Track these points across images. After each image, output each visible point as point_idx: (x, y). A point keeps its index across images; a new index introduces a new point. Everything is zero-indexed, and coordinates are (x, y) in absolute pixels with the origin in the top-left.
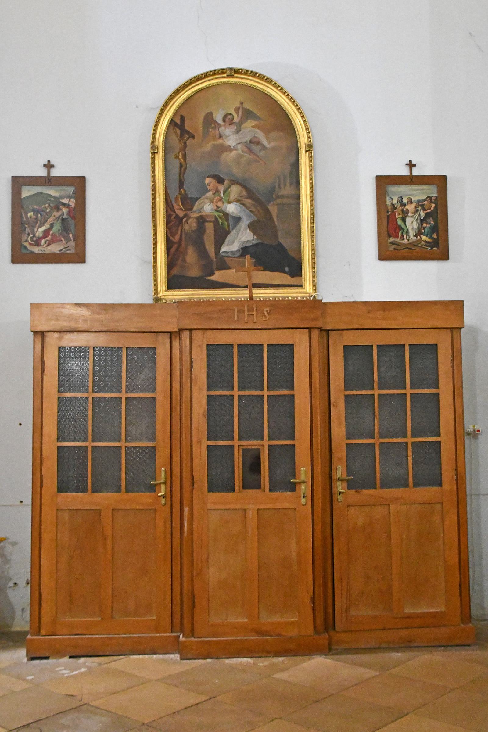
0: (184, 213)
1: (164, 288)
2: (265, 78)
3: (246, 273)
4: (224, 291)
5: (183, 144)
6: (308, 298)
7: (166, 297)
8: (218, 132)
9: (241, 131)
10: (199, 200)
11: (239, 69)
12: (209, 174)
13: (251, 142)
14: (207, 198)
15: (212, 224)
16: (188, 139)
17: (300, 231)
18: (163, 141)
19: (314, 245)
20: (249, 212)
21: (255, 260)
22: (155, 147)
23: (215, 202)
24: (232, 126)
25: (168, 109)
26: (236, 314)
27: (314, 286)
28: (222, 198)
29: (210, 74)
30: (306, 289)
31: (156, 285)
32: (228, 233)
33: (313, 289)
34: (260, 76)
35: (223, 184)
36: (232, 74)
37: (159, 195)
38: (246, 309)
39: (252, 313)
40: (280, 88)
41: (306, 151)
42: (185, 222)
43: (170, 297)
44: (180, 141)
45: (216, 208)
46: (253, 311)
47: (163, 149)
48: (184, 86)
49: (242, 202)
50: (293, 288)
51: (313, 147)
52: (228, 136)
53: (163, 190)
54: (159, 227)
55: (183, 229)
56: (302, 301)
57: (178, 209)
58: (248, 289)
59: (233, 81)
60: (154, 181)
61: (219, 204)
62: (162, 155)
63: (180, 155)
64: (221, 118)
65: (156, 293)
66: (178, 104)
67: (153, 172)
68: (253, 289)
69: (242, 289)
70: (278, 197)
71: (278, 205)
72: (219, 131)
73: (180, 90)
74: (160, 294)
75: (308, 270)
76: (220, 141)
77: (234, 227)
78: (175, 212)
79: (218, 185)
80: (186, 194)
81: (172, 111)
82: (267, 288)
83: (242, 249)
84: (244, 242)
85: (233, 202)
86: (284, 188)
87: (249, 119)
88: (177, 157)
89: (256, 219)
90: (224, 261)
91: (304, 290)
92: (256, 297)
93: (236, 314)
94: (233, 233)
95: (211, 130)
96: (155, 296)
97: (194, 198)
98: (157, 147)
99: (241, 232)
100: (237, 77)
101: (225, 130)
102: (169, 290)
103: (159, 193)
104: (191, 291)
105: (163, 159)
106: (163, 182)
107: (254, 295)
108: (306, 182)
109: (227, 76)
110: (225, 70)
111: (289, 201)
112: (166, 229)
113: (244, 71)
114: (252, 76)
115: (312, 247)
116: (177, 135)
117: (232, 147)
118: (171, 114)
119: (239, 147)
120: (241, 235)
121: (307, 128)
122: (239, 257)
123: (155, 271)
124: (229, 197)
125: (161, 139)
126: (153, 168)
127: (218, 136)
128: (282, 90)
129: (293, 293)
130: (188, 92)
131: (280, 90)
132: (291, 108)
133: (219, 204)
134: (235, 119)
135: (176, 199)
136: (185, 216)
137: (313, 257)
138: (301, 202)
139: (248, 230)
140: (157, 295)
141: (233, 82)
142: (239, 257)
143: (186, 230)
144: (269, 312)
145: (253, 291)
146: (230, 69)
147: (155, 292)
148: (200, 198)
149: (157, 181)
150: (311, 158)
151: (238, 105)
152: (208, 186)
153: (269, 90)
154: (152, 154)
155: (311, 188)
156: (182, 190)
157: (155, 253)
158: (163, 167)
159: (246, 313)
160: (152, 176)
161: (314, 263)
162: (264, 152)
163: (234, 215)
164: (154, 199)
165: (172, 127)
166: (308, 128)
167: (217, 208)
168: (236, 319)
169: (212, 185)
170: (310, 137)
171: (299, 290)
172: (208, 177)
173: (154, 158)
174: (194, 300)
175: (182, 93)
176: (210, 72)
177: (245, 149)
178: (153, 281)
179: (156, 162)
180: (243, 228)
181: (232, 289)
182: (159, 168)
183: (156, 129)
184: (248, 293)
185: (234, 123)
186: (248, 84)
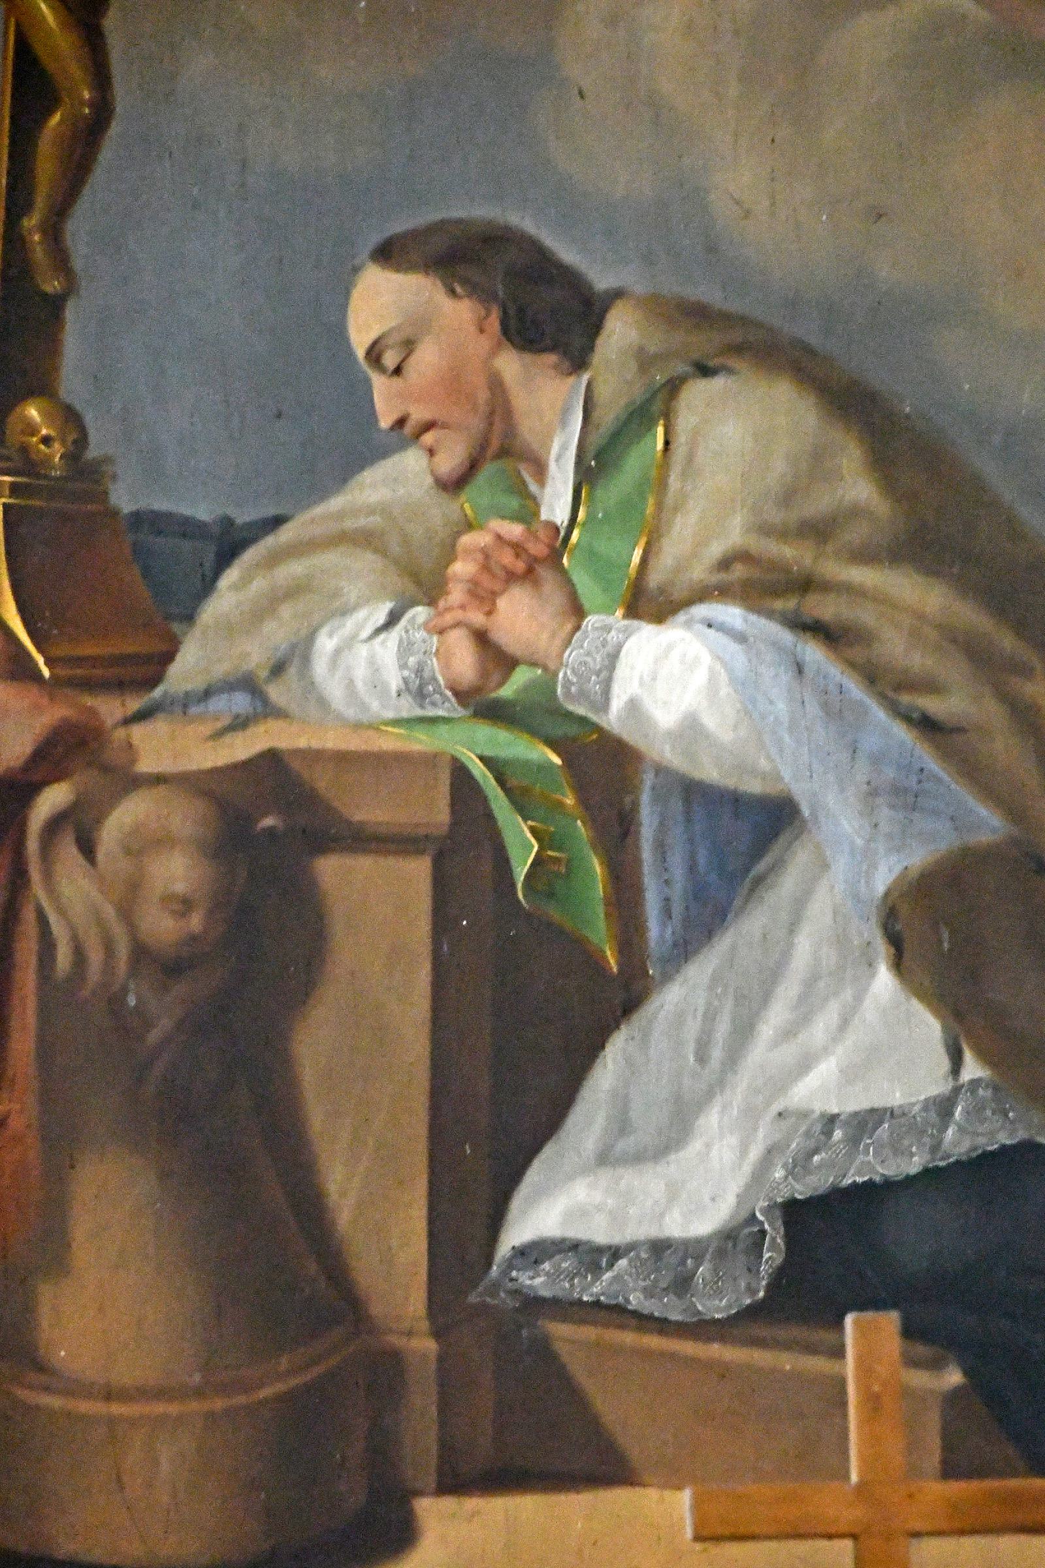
0: (53, 714)
3: (848, 1544)
10: (250, 555)
12: (399, 226)
14: (366, 540)
20: (901, 733)
21: (954, 1377)
23: (456, 594)
28: (558, 541)
35: (578, 361)
49: (826, 608)
79: (510, 364)
84: (831, 1120)
85: (702, 594)
90: (544, 1350)
97: (188, 528)
99: (788, 991)
120: (788, 1033)
139: (884, 980)
152: (379, 384)
163: (709, 772)
167: (484, 674)
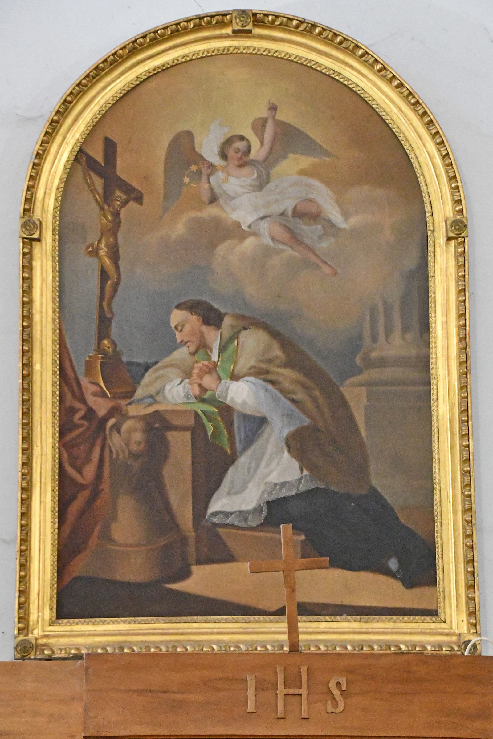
0: (110, 404)
1: (48, 614)
2: (339, 39)
4: (218, 625)
5: (110, 218)
6: (456, 648)
7: (52, 641)
8: (206, 186)
9: (271, 185)
11: (267, 15)
12: (180, 301)
13: (297, 214)
15: (188, 435)
16: (125, 203)
17: (431, 457)
18: (55, 208)
19: (470, 496)
20: (288, 403)
22: (34, 223)
23: (195, 376)
24: (246, 170)
25: (69, 120)
26: (251, 692)
27: (472, 614)
28: (215, 365)
29: (185, 28)
30: (448, 621)
31: (23, 606)
32: (232, 460)
33: (469, 623)
34: (325, 34)
36: (249, 27)
37: (42, 355)
38: (280, 679)
39: (297, 691)
40: (379, 67)
41: (449, 239)
42: (112, 427)
43: (62, 641)
44: (102, 209)
45: (197, 391)
46: (300, 688)
47: (54, 230)
48: (114, 61)
49: (271, 377)
50: (412, 618)
51: (469, 227)
52: (233, 198)
53: (54, 341)
54: (39, 444)
55: (107, 448)
56: (438, 658)
57: (95, 394)
58: (285, 618)
59: (248, 48)
60: (27, 317)
61: (208, 381)
62: (53, 247)
63: (103, 245)
64: (216, 149)
65: (24, 629)
66: (97, 108)
67: (28, 291)
68: (299, 617)
69: (267, 618)
70: (370, 364)
71: (368, 384)
72: (209, 182)
73: (103, 70)
74: (35, 632)
75: (452, 567)
76: (212, 211)
77: (249, 442)
78: (83, 400)
79: (204, 329)
80: (117, 354)
81: (82, 128)
82: (338, 618)
83: (269, 504)
84: (276, 484)
86: (387, 336)
87: (294, 152)
88: (94, 253)
89: (307, 421)
90: (218, 535)
91: (443, 625)
92: (307, 641)
93: (251, 692)
94: (243, 460)
95: (186, 180)
96: (22, 637)
97: (138, 365)
98: (38, 223)
100: (261, 37)
101: (226, 181)
102: (60, 621)
103: (42, 350)
104: (124, 622)
105: (53, 257)
106: (54, 320)
107: (301, 637)
108: (446, 324)
109: (234, 32)
110: (228, 17)
111: (399, 373)
112: (59, 448)
113: (280, 19)
114: (301, 34)
115: (463, 502)
116: (93, 191)
117: (244, 227)
118: (77, 136)
119: (264, 226)
120: (267, 466)
121: (451, 174)
122: (260, 527)
123: (24, 566)
124: (235, 363)
125: (51, 203)
126: (28, 280)
127: (205, 196)
128: (383, 73)
129: (411, 633)
130: (126, 75)
131: (380, 71)
132: (409, 120)
133: (208, 381)
134: (253, 151)
135: (89, 365)
136: (114, 411)
137: (468, 532)
138: (433, 377)
139: (286, 454)
140: (27, 635)
141: (251, 51)
142: (260, 527)
143: (113, 449)
144: (344, 688)
145: (300, 625)
146: (243, 13)
147: (21, 625)
148: (156, 363)
149: (37, 318)
150: (461, 259)
151: (264, 113)
153: (347, 73)
154: (24, 243)
155: (463, 339)
156: (106, 342)
157: (26, 515)
158: (54, 277)
159: (281, 689)
160: (24, 303)
161: (472, 547)
162: (332, 240)
163: (249, 412)
164: (27, 365)
165: (79, 172)
166: (455, 177)
168: (251, 708)
169: (187, 328)
170: (460, 200)
171: (428, 624)
172: (178, 307)
173: (30, 253)
174: (131, 648)
175: (108, 79)
176: (188, 21)
177: (279, 231)
178: (17, 595)
179: (37, 264)
180: (270, 448)
181: (240, 617)
182: (43, 280)
183: (37, 174)
184: (286, 630)
185: (252, 161)
186: (290, 56)
